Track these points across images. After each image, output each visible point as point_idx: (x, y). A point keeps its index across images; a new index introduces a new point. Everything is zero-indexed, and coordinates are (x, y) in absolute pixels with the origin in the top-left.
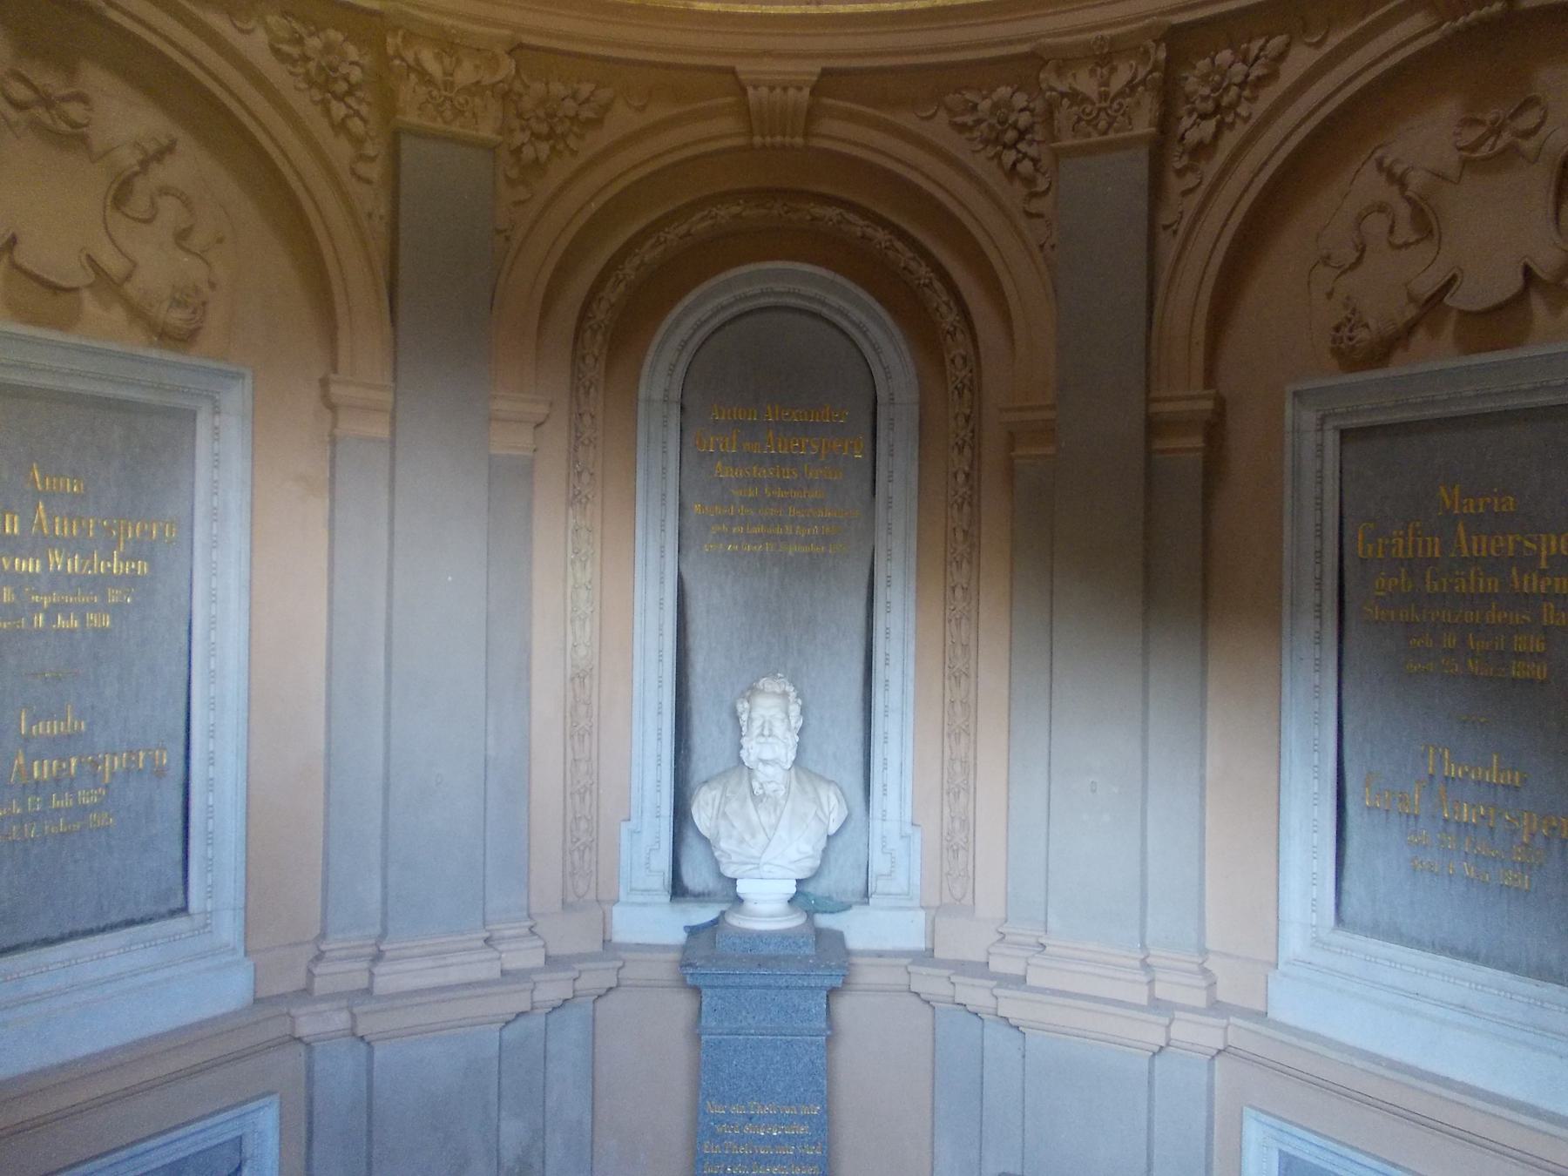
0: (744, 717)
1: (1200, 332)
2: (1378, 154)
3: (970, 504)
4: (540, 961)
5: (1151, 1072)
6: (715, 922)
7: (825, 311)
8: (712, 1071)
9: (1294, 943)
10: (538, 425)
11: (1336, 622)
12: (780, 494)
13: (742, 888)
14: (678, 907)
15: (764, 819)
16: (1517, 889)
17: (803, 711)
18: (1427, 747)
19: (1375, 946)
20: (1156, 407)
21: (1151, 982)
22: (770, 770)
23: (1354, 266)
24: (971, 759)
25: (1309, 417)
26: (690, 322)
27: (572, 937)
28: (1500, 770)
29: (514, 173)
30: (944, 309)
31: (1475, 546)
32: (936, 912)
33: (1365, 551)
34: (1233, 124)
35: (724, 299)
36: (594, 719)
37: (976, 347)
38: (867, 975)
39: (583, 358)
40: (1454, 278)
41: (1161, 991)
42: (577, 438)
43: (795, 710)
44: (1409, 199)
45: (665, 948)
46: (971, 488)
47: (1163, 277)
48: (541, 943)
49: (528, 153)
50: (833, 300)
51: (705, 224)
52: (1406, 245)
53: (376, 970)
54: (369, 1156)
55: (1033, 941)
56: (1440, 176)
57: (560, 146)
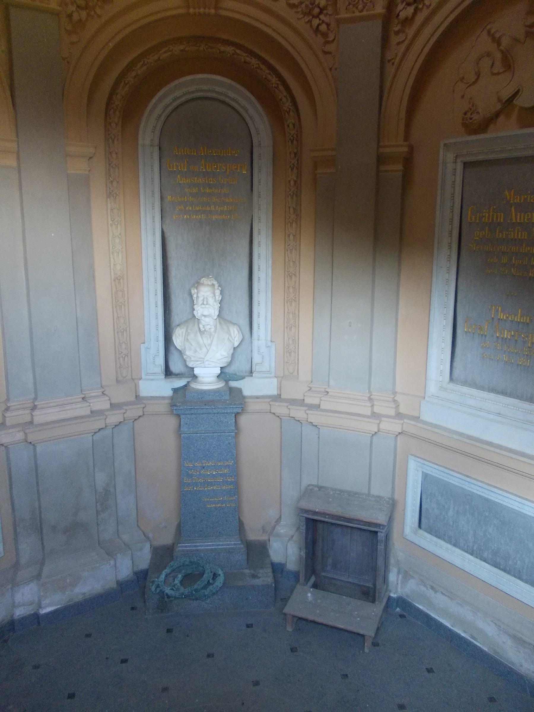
0: (195, 296)
1: (403, 113)
2: (488, 27)
3: (296, 196)
4: (108, 406)
5: (371, 442)
6: (185, 386)
7: (227, 100)
8: (186, 448)
9: (432, 388)
10: (91, 158)
11: (457, 254)
12: (208, 191)
13: (197, 371)
14: (168, 380)
15: (205, 341)
16: (525, 366)
17: (222, 293)
18: (492, 306)
19: (466, 390)
20: (381, 150)
21: (372, 406)
22: (207, 320)
23: (474, 83)
24: (297, 312)
25: (450, 156)
26: (162, 105)
27: (121, 395)
28: (521, 317)
29: (69, 27)
30: (284, 100)
31: (518, 217)
32: (281, 379)
33: (471, 219)
34: (422, 9)
35: (177, 93)
36: (126, 298)
37: (299, 118)
38: (252, 406)
39: (110, 123)
40: (517, 92)
41: (376, 410)
42: (110, 164)
43: (218, 292)
44: (502, 52)
45: (163, 398)
46: (297, 188)
47: (388, 85)
48: (108, 398)
49: (76, 17)
50: (231, 94)
51: (166, 55)
52: (498, 74)
53: (34, 414)
54: (38, 491)
55: (323, 390)
56: (516, 40)
57: (92, 13)
